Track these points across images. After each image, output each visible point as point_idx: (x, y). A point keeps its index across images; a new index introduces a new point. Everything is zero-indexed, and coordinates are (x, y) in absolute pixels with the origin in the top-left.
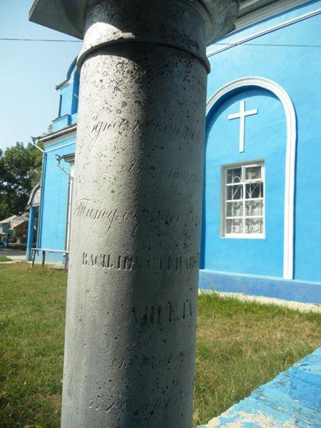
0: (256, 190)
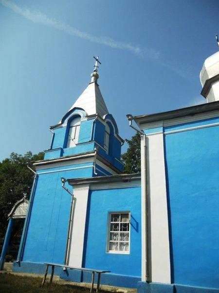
0: (125, 227)
